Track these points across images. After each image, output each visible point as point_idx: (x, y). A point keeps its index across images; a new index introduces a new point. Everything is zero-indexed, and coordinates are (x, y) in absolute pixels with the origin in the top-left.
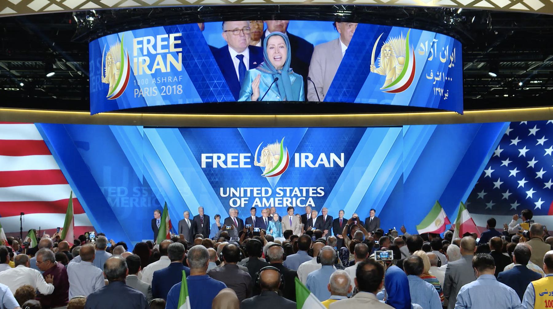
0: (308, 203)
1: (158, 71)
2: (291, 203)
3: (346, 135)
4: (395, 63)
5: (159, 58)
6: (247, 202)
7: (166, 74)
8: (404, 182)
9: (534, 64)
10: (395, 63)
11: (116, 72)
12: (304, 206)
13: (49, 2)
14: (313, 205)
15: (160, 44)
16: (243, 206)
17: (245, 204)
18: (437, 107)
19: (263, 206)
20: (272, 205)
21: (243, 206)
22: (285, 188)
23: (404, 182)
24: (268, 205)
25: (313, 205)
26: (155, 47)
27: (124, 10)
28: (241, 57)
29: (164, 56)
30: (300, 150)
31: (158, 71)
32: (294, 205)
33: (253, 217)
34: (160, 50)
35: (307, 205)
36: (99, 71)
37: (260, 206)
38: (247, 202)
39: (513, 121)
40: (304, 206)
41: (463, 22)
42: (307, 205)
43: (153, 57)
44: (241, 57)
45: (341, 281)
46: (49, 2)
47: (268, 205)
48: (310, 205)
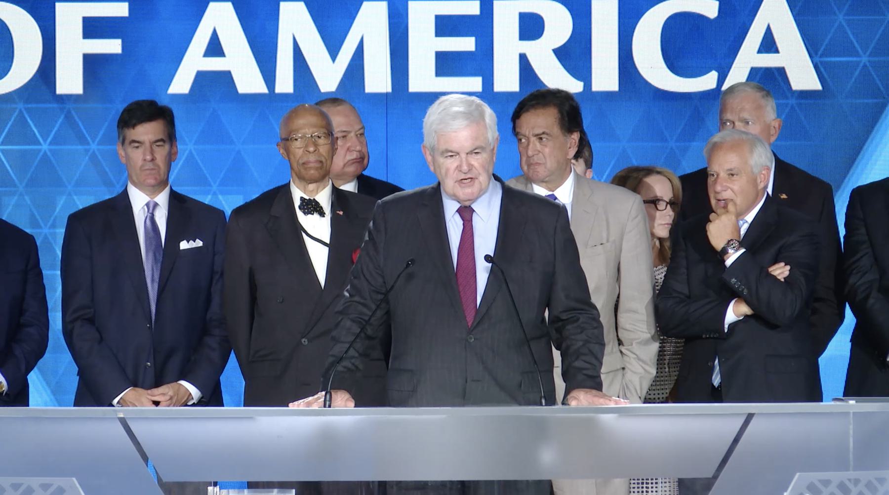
0: (748, 58)
2: (576, 55)
6: (112, 46)
8: (847, 305)
12: (707, 82)
13: (328, 242)
14: (804, 77)
16: (70, 80)
17: (91, 62)
19: (285, 83)
20: (378, 79)
21: (70, 80)
23: (847, 305)
24: (328, 75)
25: (804, 77)
28: (466, 212)
32: (605, 76)
33: (138, 199)
35: (738, 74)
37: (249, 80)
38: (112, 46)
40: (707, 82)
42: (738, 74)
44: (466, 212)
46: (328, 242)
47: (328, 75)
48: (770, 81)
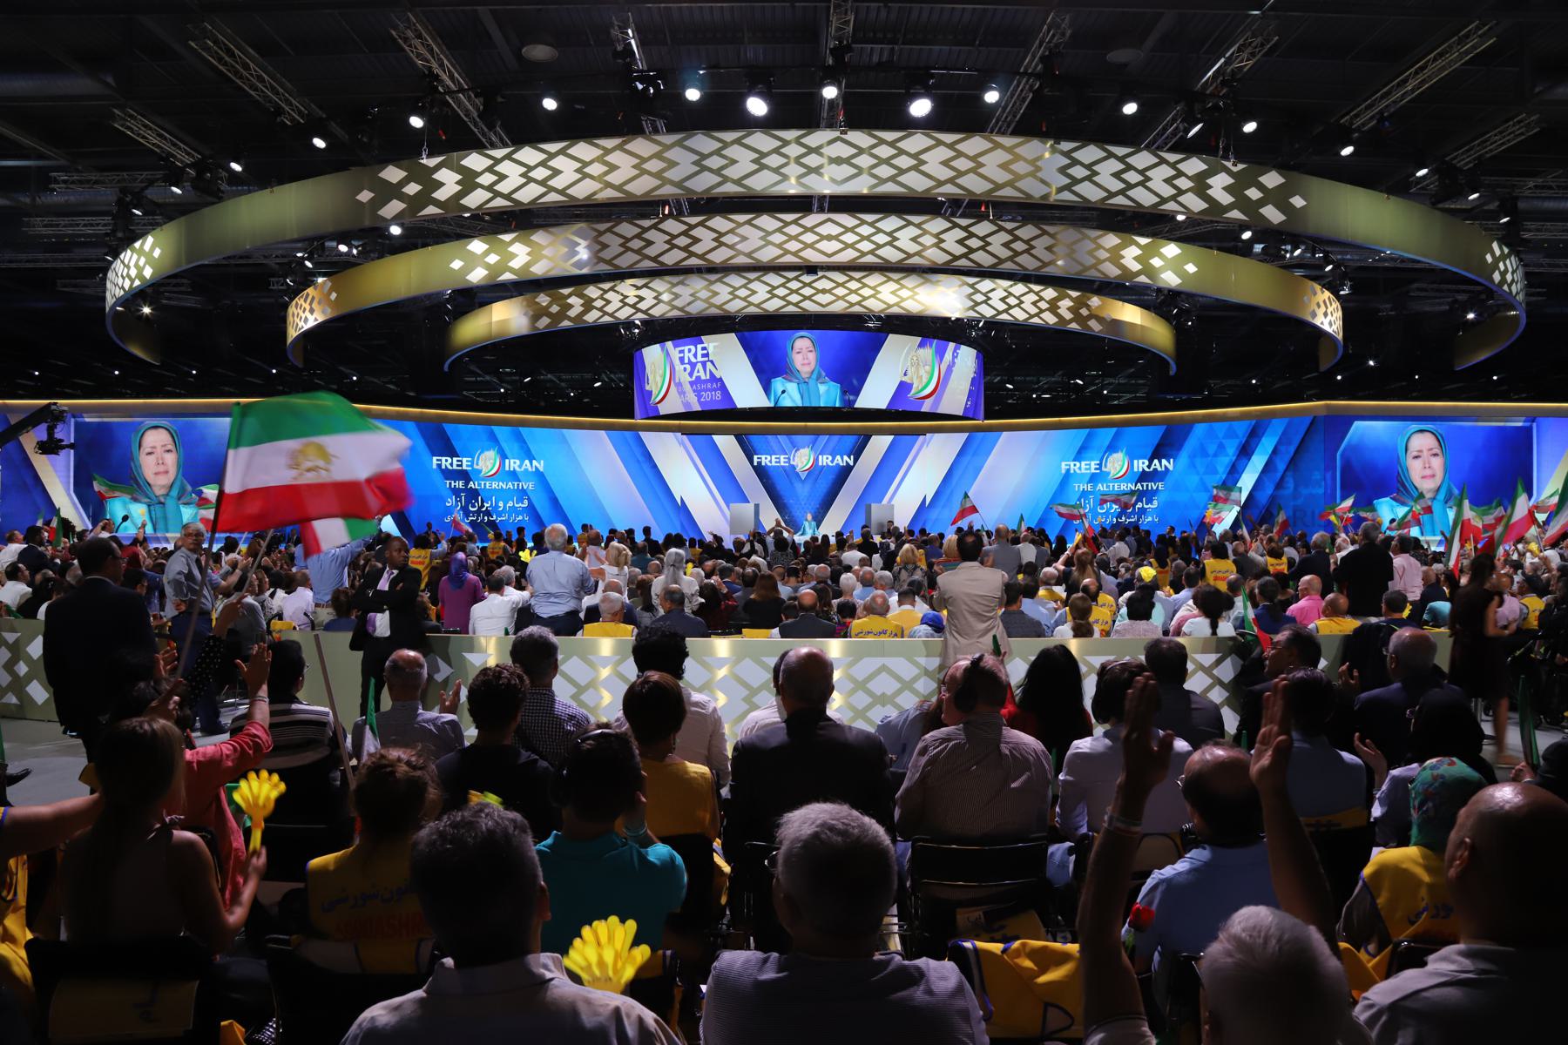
1: (698, 378)
3: (850, 441)
4: (922, 372)
5: (699, 366)
7: (706, 381)
9: (1044, 380)
10: (922, 372)
11: (659, 380)
15: (700, 352)
18: (960, 413)
22: (1150, 42)
26: (695, 355)
27: (669, 319)
29: (704, 364)
30: (987, 364)
31: (698, 378)
34: (700, 358)
36: (643, 378)
39: (409, 479)
41: (984, 336)
43: (693, 365)
45: (879, 600)
